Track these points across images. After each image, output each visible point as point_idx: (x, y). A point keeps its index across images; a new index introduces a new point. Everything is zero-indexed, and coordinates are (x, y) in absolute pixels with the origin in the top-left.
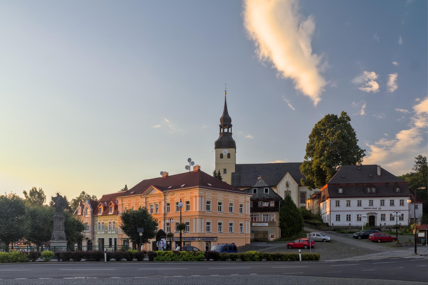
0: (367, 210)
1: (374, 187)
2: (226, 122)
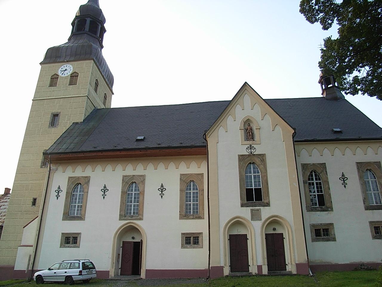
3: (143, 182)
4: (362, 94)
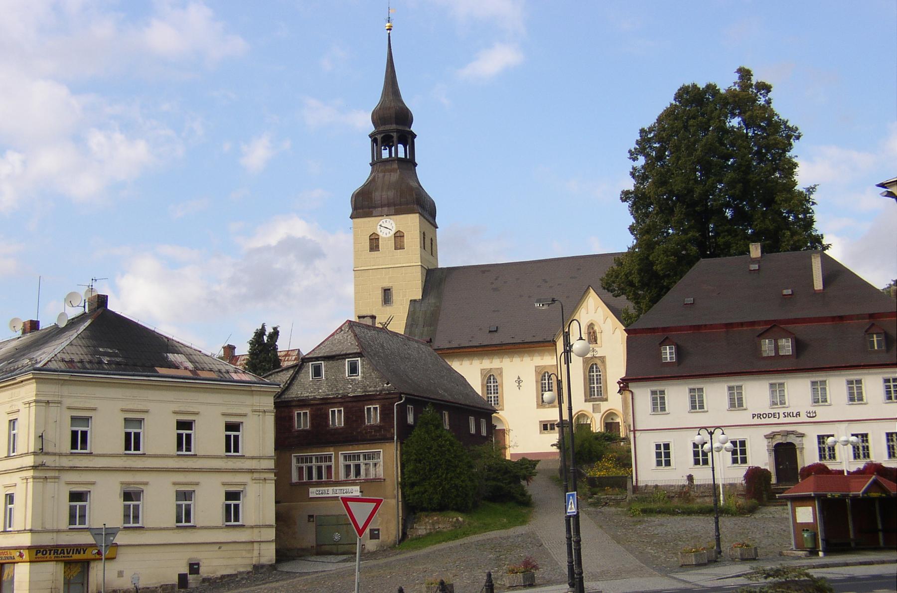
0: (767, 421)
1: (787, 334)
2: (394, 126)
3: (501, 374)
4: (269, 330)
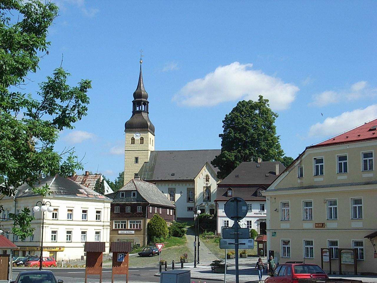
2: (140, 100)
